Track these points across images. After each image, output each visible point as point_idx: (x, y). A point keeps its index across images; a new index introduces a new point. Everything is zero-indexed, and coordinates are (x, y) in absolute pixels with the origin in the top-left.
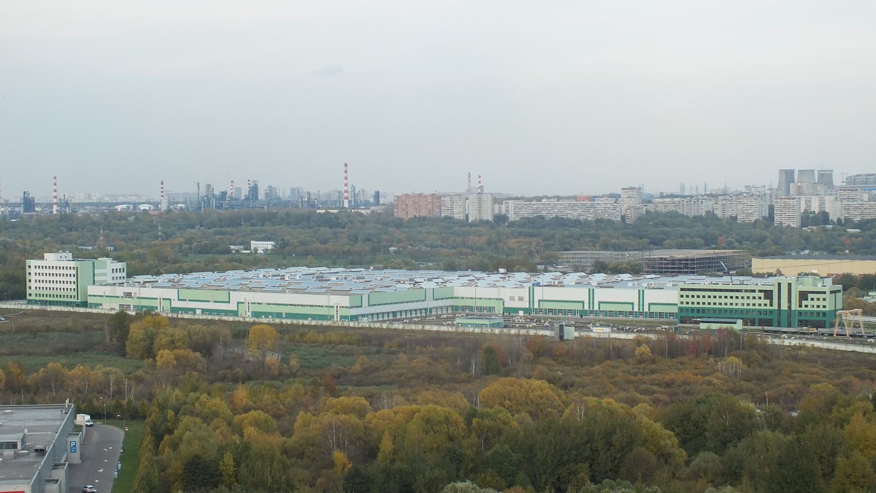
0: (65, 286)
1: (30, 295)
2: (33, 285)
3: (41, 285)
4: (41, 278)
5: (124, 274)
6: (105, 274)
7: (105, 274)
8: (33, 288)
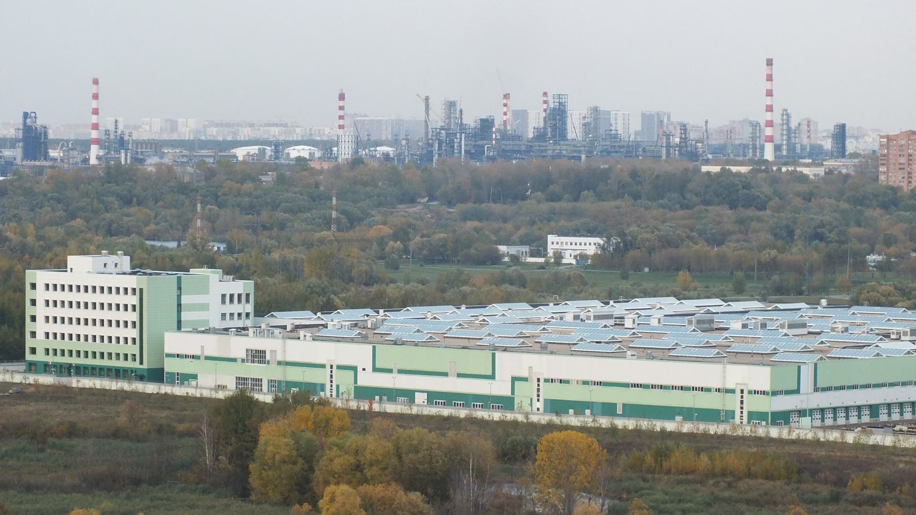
0: (114, 332)
1: (33, 351)
2: (41, 327)
3: (59, 328)
4: (59, 312)
5: (250, 308)
6: (204, 307)
7: (204, 307)
8: (40, 336)
